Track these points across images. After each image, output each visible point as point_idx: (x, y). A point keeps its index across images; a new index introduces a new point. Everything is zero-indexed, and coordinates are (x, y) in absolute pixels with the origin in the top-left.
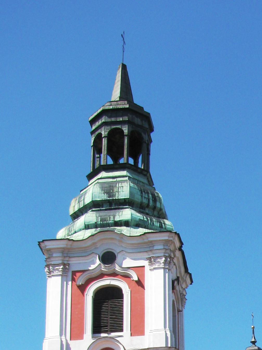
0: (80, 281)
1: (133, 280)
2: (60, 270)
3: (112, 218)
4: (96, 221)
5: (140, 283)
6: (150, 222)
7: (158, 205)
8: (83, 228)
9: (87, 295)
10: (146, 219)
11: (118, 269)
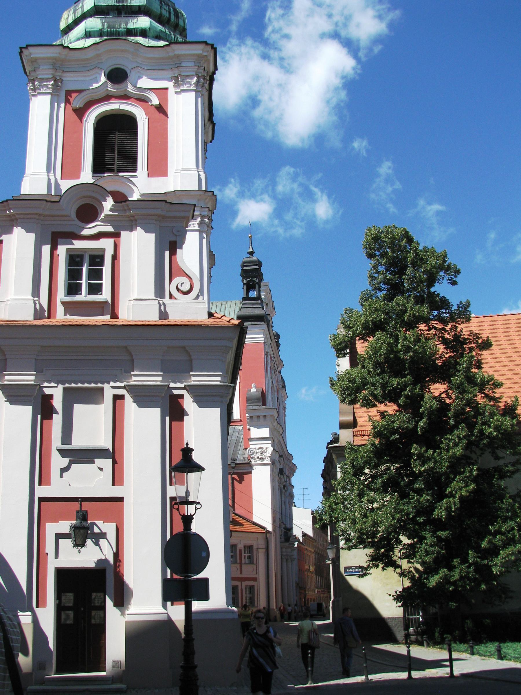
0: (78, 102)
1: (152, 105)
2: (50, 86)
3: (123, 25)
4: (100, 27)
5: (161, 109)
6: (173, 37)
7: (181, 23)
8: (83, 36)
9: (86, 121)
10: (168, 32)
11: (130, 88)
